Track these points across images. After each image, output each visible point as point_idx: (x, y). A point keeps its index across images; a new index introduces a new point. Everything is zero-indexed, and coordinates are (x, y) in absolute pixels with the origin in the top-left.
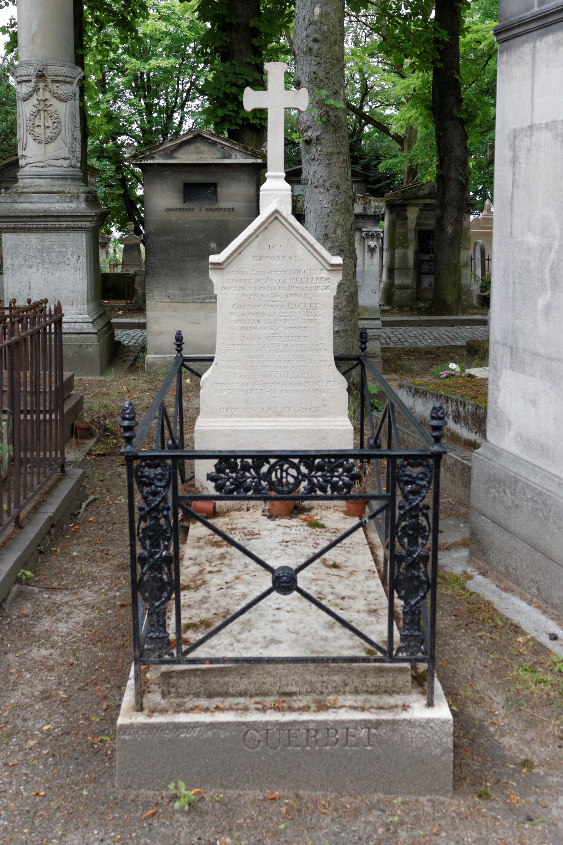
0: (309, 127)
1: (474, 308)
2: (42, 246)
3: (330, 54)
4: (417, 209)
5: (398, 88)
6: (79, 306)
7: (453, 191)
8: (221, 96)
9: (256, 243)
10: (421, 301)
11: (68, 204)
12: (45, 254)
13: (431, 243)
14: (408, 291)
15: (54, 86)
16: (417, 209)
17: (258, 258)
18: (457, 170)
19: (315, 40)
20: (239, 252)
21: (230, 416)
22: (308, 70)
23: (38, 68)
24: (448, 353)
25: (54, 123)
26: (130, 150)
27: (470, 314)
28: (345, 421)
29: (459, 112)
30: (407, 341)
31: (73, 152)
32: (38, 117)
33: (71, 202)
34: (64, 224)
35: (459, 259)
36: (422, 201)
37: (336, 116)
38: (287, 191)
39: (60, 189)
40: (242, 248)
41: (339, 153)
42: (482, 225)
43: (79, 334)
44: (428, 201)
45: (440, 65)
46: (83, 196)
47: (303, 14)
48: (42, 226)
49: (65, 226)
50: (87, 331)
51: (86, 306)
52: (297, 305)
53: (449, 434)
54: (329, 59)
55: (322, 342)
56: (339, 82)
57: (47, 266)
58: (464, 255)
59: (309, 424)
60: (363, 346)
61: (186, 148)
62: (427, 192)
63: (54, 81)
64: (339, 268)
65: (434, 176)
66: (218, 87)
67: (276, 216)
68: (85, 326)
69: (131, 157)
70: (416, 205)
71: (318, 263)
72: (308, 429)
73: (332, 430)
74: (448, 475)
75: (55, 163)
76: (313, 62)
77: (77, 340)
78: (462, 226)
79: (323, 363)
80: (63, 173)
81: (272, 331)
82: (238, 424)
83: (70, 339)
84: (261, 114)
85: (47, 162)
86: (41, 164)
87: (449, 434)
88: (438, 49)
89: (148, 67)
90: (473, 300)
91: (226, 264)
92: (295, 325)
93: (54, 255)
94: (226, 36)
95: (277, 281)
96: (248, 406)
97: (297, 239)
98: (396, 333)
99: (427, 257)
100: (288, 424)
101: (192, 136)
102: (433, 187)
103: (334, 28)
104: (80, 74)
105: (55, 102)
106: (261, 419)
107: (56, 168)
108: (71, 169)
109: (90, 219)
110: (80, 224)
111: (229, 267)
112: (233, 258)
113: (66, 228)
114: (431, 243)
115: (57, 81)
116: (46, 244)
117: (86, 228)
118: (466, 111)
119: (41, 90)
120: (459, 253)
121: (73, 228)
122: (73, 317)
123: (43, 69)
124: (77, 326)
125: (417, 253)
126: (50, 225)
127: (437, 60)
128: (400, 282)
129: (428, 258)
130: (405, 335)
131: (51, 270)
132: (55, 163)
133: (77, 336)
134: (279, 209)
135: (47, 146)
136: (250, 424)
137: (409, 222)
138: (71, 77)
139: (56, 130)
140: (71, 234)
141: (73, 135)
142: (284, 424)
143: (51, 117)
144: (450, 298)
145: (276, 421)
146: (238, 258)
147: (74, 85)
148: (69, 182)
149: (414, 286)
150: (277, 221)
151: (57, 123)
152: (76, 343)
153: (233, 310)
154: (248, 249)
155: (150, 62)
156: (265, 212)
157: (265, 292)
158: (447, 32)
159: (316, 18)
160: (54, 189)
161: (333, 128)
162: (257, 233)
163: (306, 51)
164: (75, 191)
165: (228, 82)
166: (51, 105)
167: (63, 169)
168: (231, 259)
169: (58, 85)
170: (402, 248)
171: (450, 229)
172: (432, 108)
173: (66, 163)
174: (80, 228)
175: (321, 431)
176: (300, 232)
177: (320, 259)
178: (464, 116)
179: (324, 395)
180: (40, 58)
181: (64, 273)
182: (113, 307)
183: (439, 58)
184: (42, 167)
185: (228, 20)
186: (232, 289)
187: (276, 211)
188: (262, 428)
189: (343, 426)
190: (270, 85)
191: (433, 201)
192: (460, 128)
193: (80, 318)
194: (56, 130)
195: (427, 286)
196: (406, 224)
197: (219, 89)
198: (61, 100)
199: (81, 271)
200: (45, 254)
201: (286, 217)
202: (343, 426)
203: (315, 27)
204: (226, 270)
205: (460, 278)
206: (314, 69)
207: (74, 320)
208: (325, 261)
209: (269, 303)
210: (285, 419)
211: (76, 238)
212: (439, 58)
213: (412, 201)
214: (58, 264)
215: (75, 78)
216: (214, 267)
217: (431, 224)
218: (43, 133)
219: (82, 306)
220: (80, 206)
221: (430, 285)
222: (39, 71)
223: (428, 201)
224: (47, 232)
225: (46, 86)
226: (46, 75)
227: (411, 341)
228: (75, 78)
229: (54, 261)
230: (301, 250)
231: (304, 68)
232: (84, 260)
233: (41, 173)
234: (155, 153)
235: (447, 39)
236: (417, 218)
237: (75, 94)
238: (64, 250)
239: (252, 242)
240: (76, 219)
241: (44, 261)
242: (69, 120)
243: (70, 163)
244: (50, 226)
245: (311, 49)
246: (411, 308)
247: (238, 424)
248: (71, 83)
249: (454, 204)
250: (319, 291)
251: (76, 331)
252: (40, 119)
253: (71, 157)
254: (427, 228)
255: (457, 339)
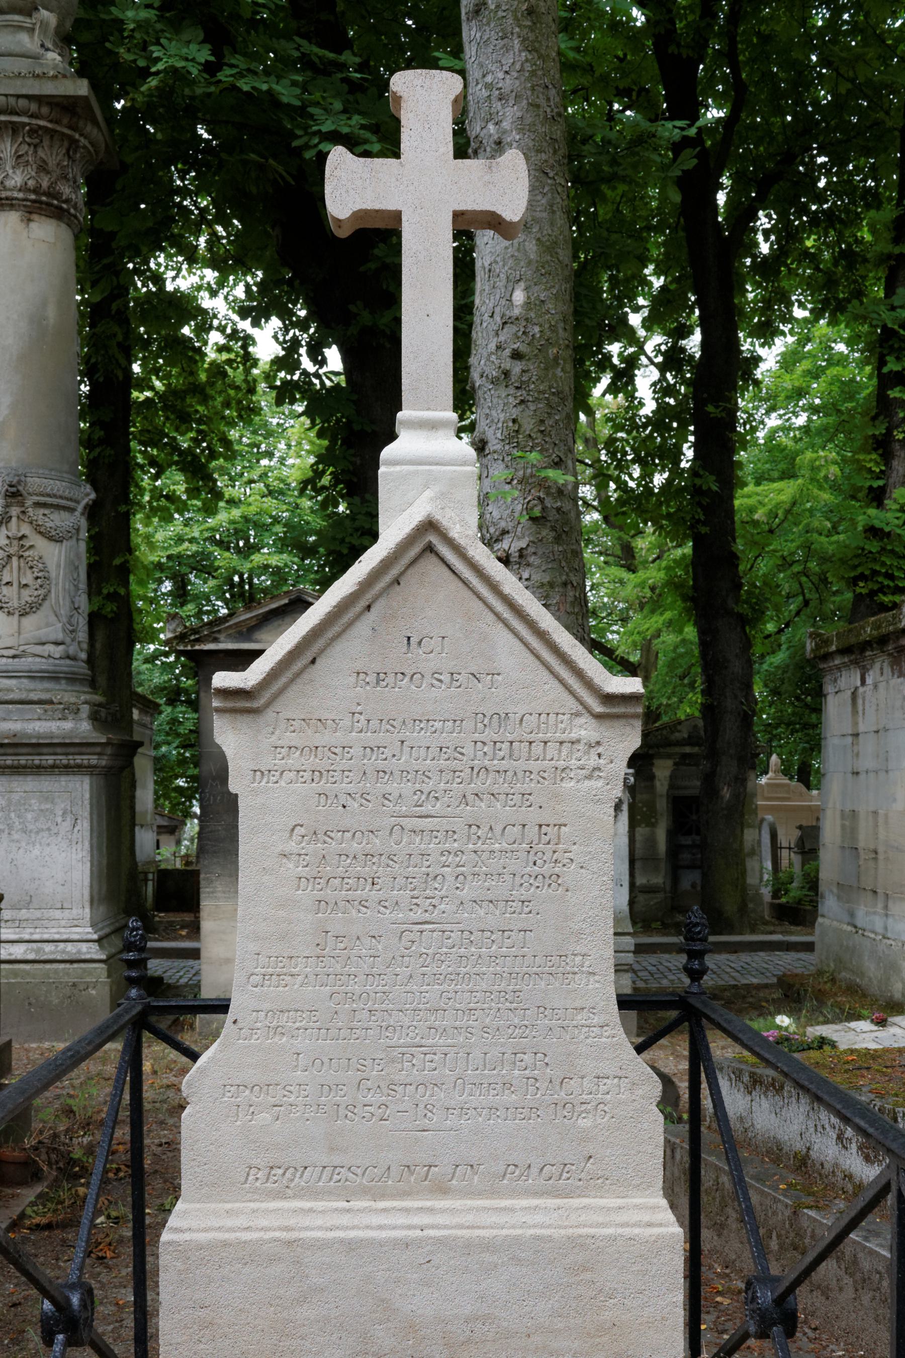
0: (504, 532)
1: (766, 923)
2: (9, 800)
3: (546, 384)
4: (670, 763)
5: (629, 587)
6: (74, 911)
7: (730, 730)
8: (345, 551)
9: (363, 628)
10: (680, 912)
11: (59, 723)
12: (13, 815)
13: (694, 817)
14: (658, 895)
15: (38, 514)
16: (670, 763)
17: (371, 678)
18: (736, 697)
19: (516, 355)
20: (309, 656)
21: (280, 1195)
22: (502, 416)
23: (8, 479)
24: (744, 997)
25: (37, 578)
26: (174, 625)
27: (763, 933)
28: (654, 1208)
29: (736, 604)
30: (666, 977)
31: (72, 632)
32: (8, 567)
33: (64, 718)
34: (50, 760)
35: (742, 842)
36: (677, 750)
37: (558, 509)
38: (464, 464)
39: (44, 696)
40: (321, 643)
41: (565, 584)
42: (766, 795)
43: (71, 962)
44: (688, 750)
45: (704, 530)
46: (85, 709)
47: (491, 305)
48: (9, 762)
49: (50, 762)
50: (88, 957)
51: (87, 910)
52: (498, 829)
53: (849, 1187)
54: (544, 392)
55: (578, 949)
56: (565, 442)
57: (16, 836)
58: (749, 836)
59: (539, 1218)
60: (696, 965)
61: (276, 624)
62: (686, 736)
63: (38, 505)
64: (630, 710)
65: (698, 706)
66: (339, 536)
67: (428, 538)
68: (84, 947)
69: (176, 638)
70: (669, 756)
71: (565, 695)
72: (537, 1238)
73: (614, 1239)
74: (866, 1298)
75: (38, 649)
76: (511, 399)
77: (68, 974)
78: (745, 788)
79: (580, 1019)
80: (51, 668)
81: (418, 915)
82: (307, 1221)
83: (56, 971)
84: (379, 238)
85: (22, 648)
86: (11, 652)
87: (849, 1187)
88: (699, 504)
89: (249, 566)
90: (763, 911)
91: (267, 695)
92: (490, 895)
93: (29, 816)
94: (354, 455)
95: (434, 751)
96: (337, 1160)
97: (498, 616)
98: (645, 964)
99: (687, 841)
100: (469, 1219)
101: (286, 601)
102: (696, 726)
103: (553, 331)
104: (88, 495)
105: (41, 544)
106: (382, 1204)
107: (38, 660)
108: (68, 662)
109: (98, 750)
110: (79, 759)
111: (278, 706)
112: (289, 674)
113: (53, 766)
114: (694, 817)
115: (44, 505)
116: (15, 797)
117: (89, 766)
118: (747, 602)
119: (14, 520)
120: (742, 832)
121: (66, 767)
122: (63, 930)
123: (19, 482)
124: (70, 947)
125: (671, 835)
126: (23, 760)
127: (698, 521)
128: (644, 881)
129: (689, 842)
130: (660, 967)
131: (23, 844)
132: (38, 649)
133: (68, 966)
134: (438, 516)
135: (23, 619)
136: (345, 1220)
137: (658, 784)
138: (71, 500)
139: (41, 592)
140: (63, 778)
141: (73, 602)
142: (457, 1220)
143: (31, 568)
144: (730, 907)
145: (431, 1210)
146: (306, 676)
147: (77, 513)
148: (63, 685)
149: (668, 888)
150: (430, 562)
151: (44, 579)
152: (66, 979)
153: (292, 846)
154: (339, 648)
155: (253, 557)
156: (393, 529)
157: (394, 788)
158: (714, 478)
159: (517, 312)
160: (34, 696)
161: (553, 534)
162: (369, 596)
163: (498, 379)
164: (73, 700)
165: (357, 530)
166: (31, 547)
167: (51, 661)
168: (283, 680)
169: (46, 512)
170: (647, 826)
171: (726, 793)
172: (692, 599)
173: (58, 651)
174: (79, 766)
175: (576, 1243)
176: (507, 589)
177: (572, 681)
178: (744, 609)
179: (584, 1123)
180: (14, 465)
181: (47, 850)
182: (171, 924)
183: (702, 518)
184: (14, 657)
185: (356, 427)
186: (289, 776)
187: (429, 526)
188: (384, 1234)
189: (650, 1225)
190: (409, 138)
191: (696, 750)
192: (739, 629)
193: (76, 933)
194: (41, 592)
195: (689, 888)
196: (653, 787)
197: (342, 541)
198: (51, 539)
199: (79, 846)
200: (13, 815)
201: (462, 542)
202: (650, 1225)
203: (514, 328)
204: (270, 715)
205: (744, 873)
206: (515, 413)
207: (65, 937)
208: (589, 684)
209: (405, 822)
210: (458, 1204)
211: (71, 785)
212: (702, 518)
213: (662, 750)
214: (37, 833)
215: (78, 502)
216: (230, 704)
217: (694, 786)
218: (16, 596)
219: (80, 911)
220: (80, 727)
221: (693, 886)
222: (11, 486)
223: (688, 750)
224: (19, 774)
225: (23, 512)
226: (24, 493)
227: (672, 977)
228: (78, 502)
229: (31, 827)
230: (507, 652)
231: (494, 413)
232: (86, 825)
233: (10, 668)
234: (219, 631)
235: (715, 488)
236: (671, 777)
237: (78, 530)
238: (48, 806)
239: (351, 624)
240: (72, 750)
241: (10, 827)
242: (65, 575)
243: (67, 652)
244: (23, 762)
245: (506, 374)
246: (663, 924)
247: (307, 1221)
248: (71, 510)
249: (732, 751)
250: (568, 785)
251: (66, 957)
252: (12, 571)
253: (68, 640)
254: (687, 793)
255: (749, 973)
